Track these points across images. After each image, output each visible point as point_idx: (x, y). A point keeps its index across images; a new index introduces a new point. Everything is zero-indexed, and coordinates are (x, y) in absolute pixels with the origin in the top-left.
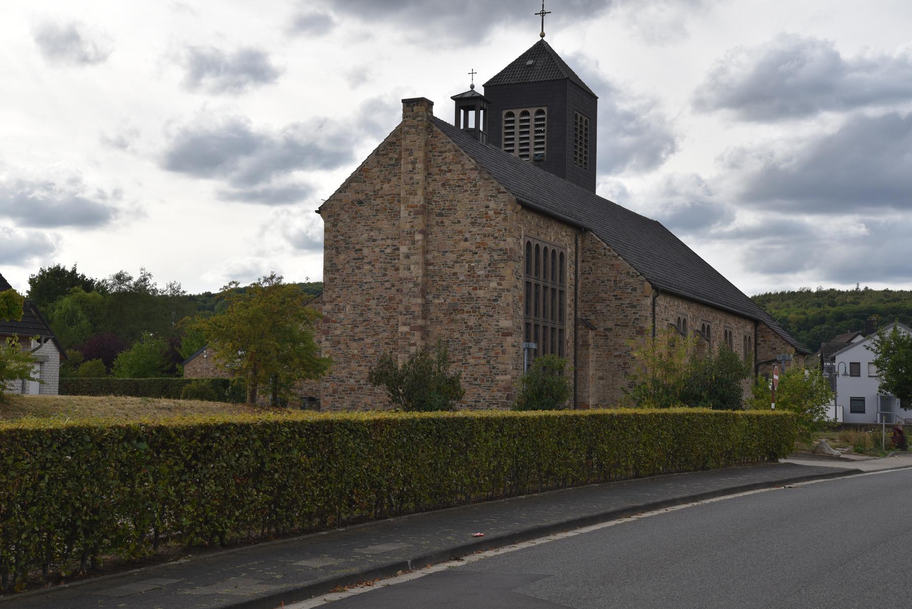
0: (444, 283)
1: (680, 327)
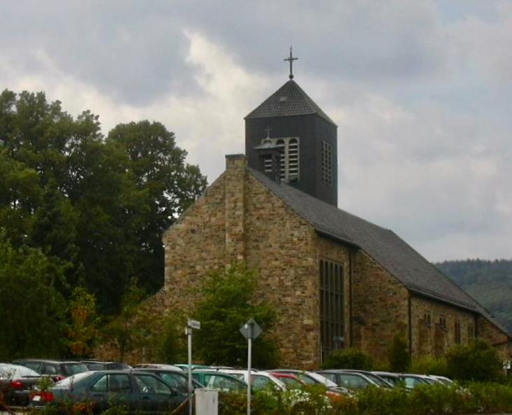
0: (261, 292)
1: (426, 321)
